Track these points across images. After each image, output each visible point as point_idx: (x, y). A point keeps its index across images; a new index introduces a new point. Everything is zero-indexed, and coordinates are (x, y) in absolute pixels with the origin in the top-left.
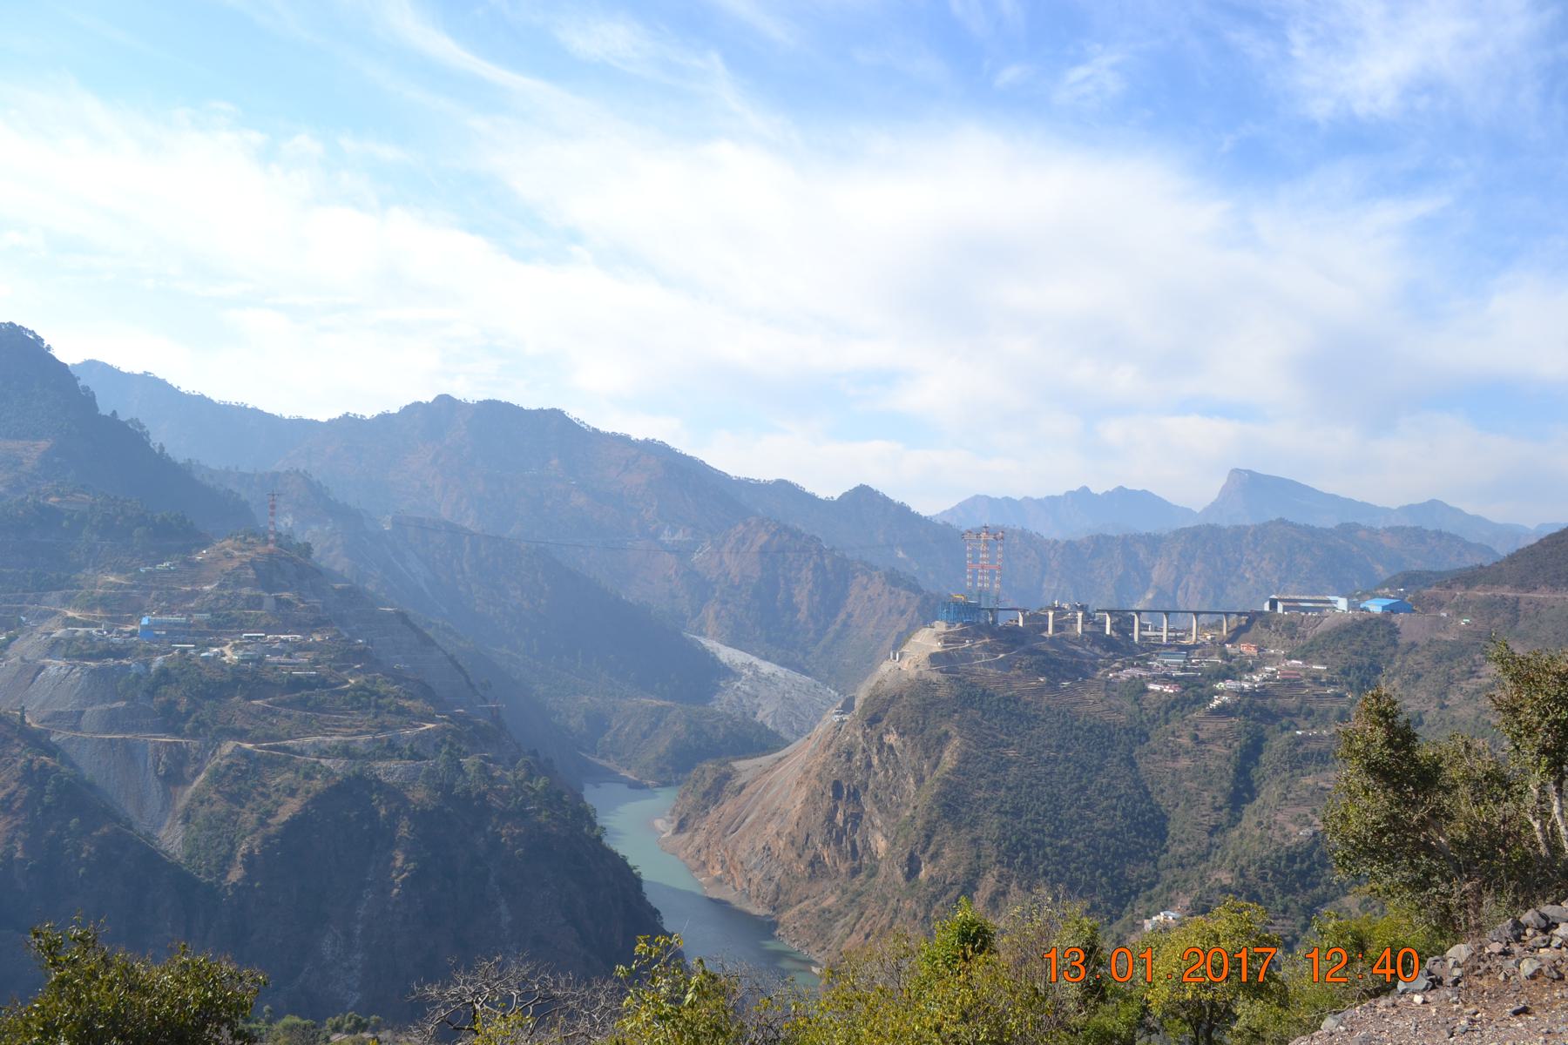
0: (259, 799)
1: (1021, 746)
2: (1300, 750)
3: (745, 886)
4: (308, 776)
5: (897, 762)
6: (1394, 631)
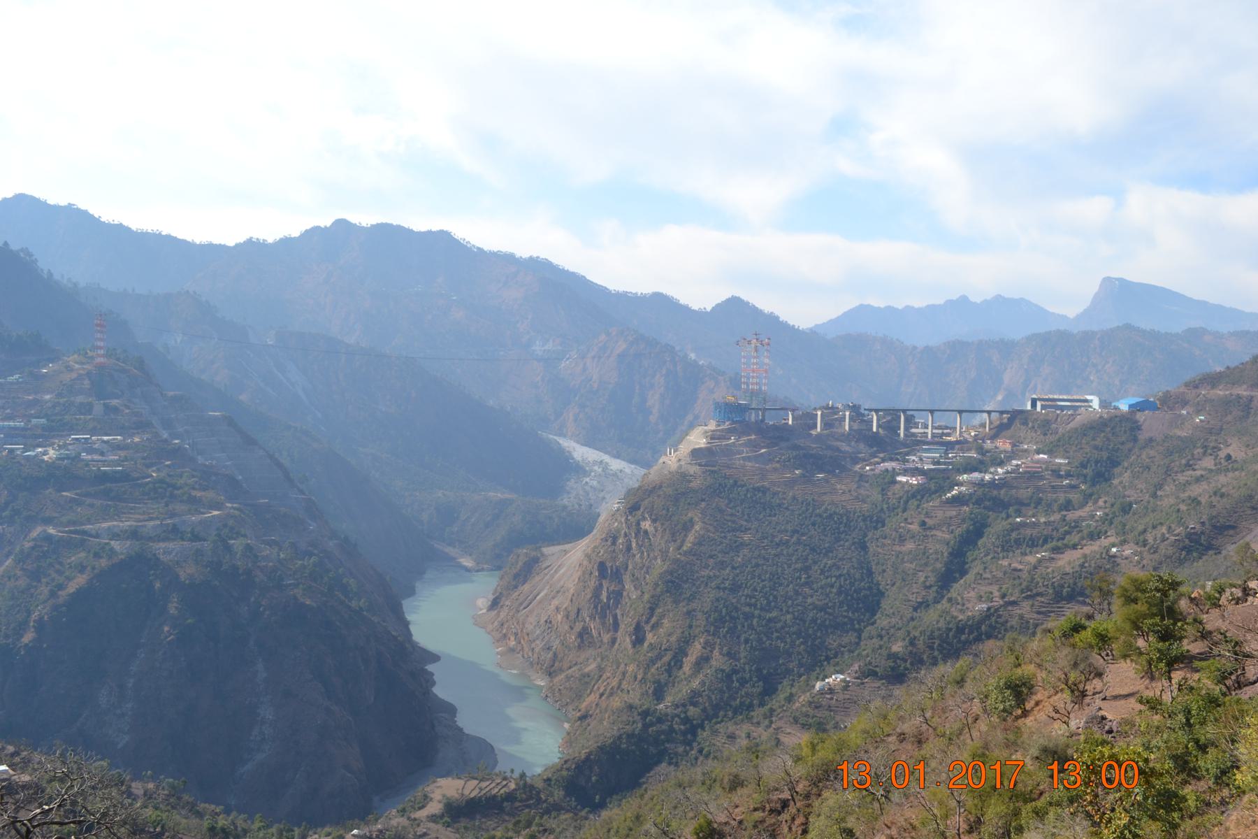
0: (54, 575)
1: (757, 531)
2: (1014, 535)
3: (530, 654)
4: (97, 556)
5: (651, 545)
6: (1136, 427)
